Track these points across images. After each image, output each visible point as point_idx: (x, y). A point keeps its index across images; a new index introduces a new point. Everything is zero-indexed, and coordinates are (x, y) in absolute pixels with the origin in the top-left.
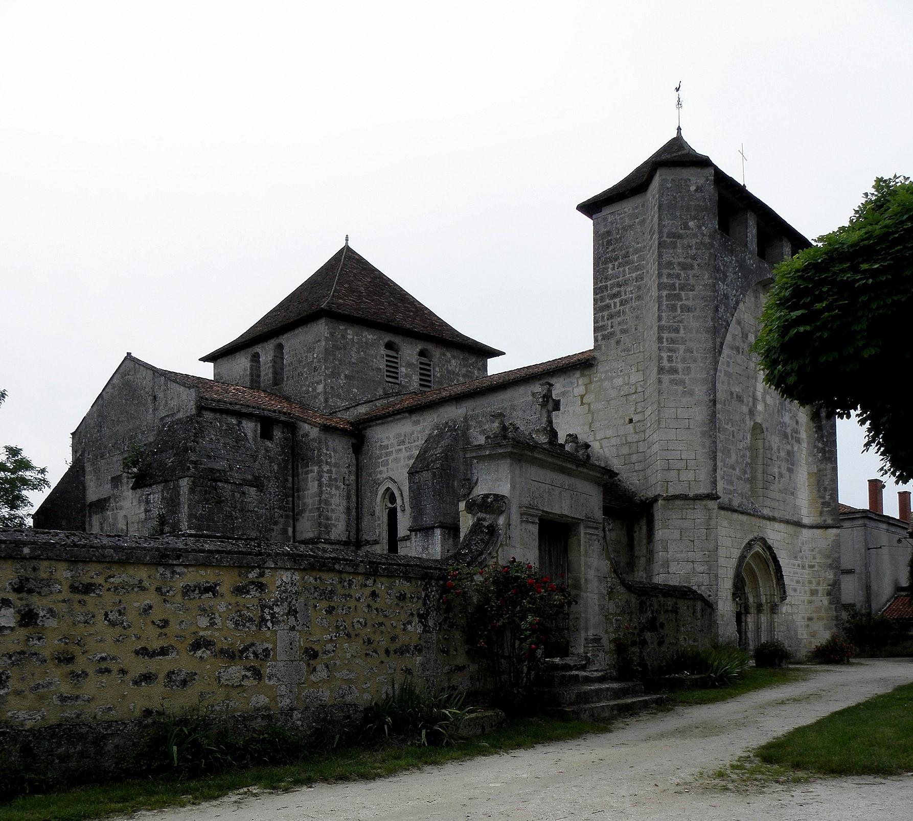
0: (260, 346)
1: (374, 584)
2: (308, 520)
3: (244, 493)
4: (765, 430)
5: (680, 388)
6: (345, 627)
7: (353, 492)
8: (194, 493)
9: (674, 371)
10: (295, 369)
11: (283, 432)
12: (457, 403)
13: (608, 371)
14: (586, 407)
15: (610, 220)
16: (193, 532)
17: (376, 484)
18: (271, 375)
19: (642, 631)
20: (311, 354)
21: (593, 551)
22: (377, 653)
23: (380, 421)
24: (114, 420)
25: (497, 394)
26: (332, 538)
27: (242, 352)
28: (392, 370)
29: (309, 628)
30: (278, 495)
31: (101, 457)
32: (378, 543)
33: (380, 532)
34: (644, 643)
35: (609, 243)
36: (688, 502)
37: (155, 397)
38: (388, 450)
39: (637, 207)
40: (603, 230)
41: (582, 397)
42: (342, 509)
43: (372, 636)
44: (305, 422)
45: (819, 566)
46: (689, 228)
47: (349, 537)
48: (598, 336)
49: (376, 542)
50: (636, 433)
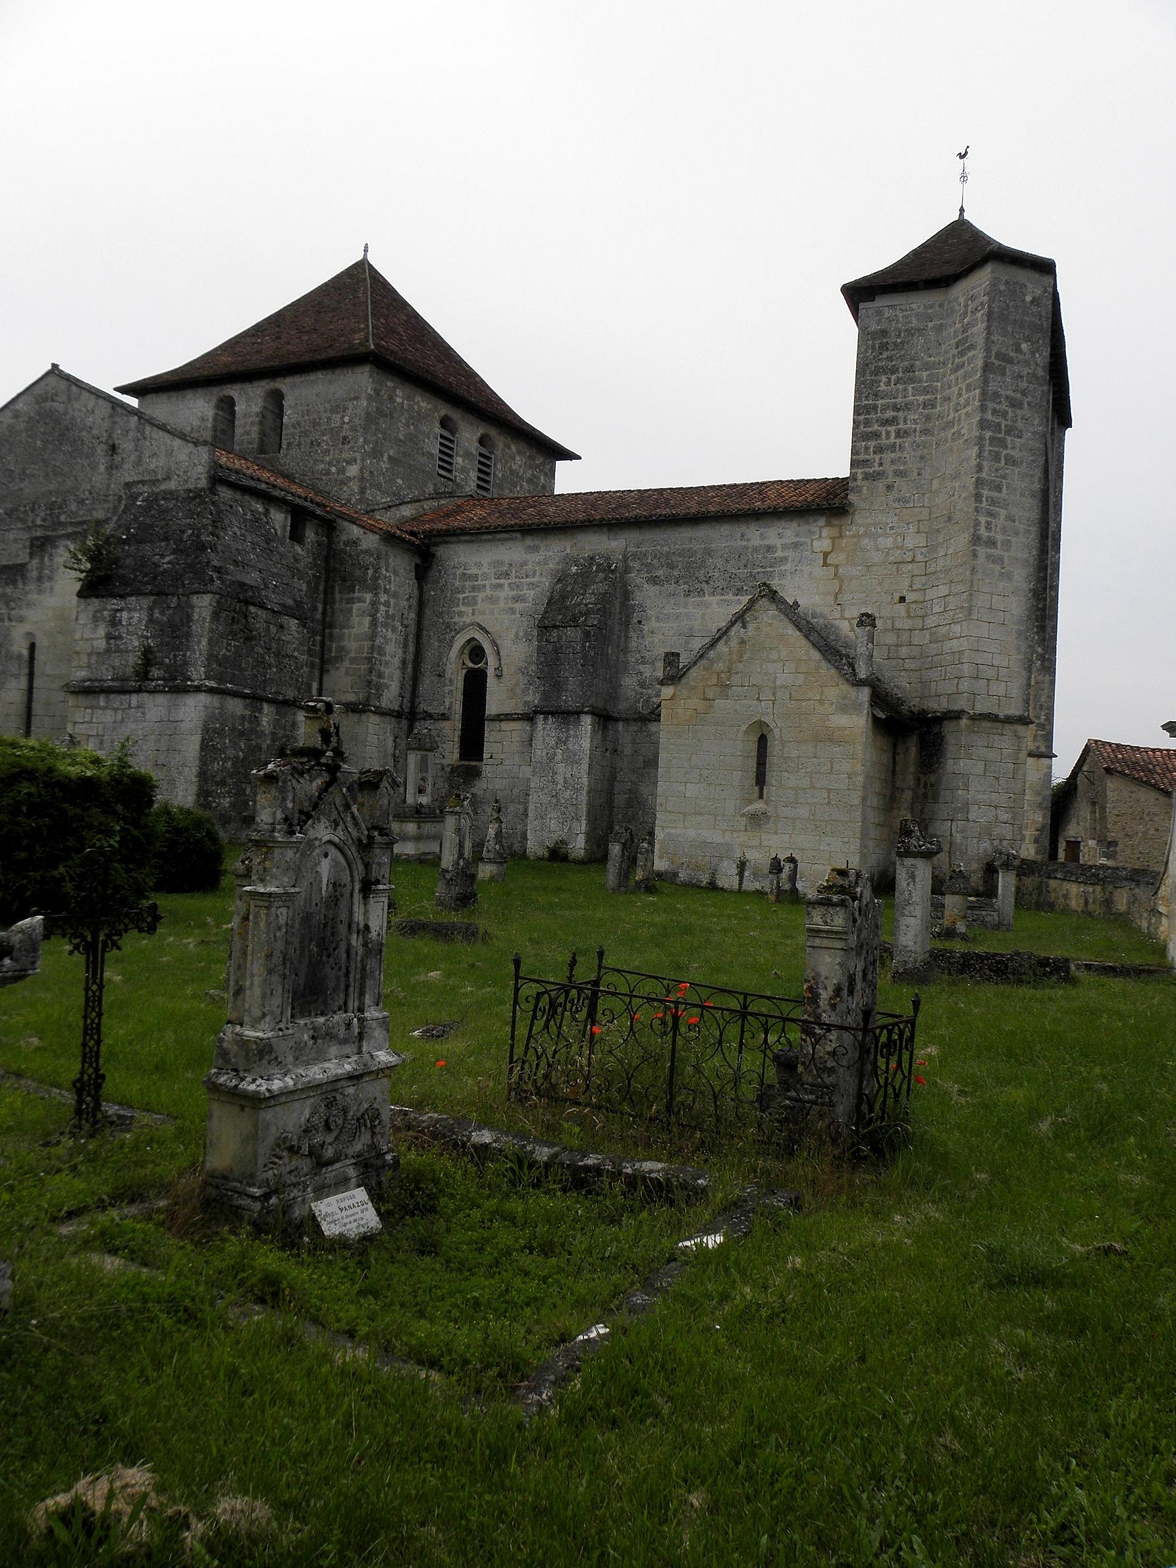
0: (237, 387)
2: (347, 674)
3: (282, 627)
7: (411, 638)
8: (218, 620)
9: (992, 543)
10: (305, 433)
11: (317, 534)
12: (609, 530)
13: (869, 525)
15: (886, 315)
16: (213, 684)
18: (255, 436)
25: (681, 529)
27: (200, 391)
32: (448, 719)
35: (884, 347)
36: (995, 724)
37: (113, 448)
39: (931, 307)
41: (826, 555)
42: (396, 661)
44: (354, 523)
47: (401, 706)
49: (444, 717)
50: (909, 617)
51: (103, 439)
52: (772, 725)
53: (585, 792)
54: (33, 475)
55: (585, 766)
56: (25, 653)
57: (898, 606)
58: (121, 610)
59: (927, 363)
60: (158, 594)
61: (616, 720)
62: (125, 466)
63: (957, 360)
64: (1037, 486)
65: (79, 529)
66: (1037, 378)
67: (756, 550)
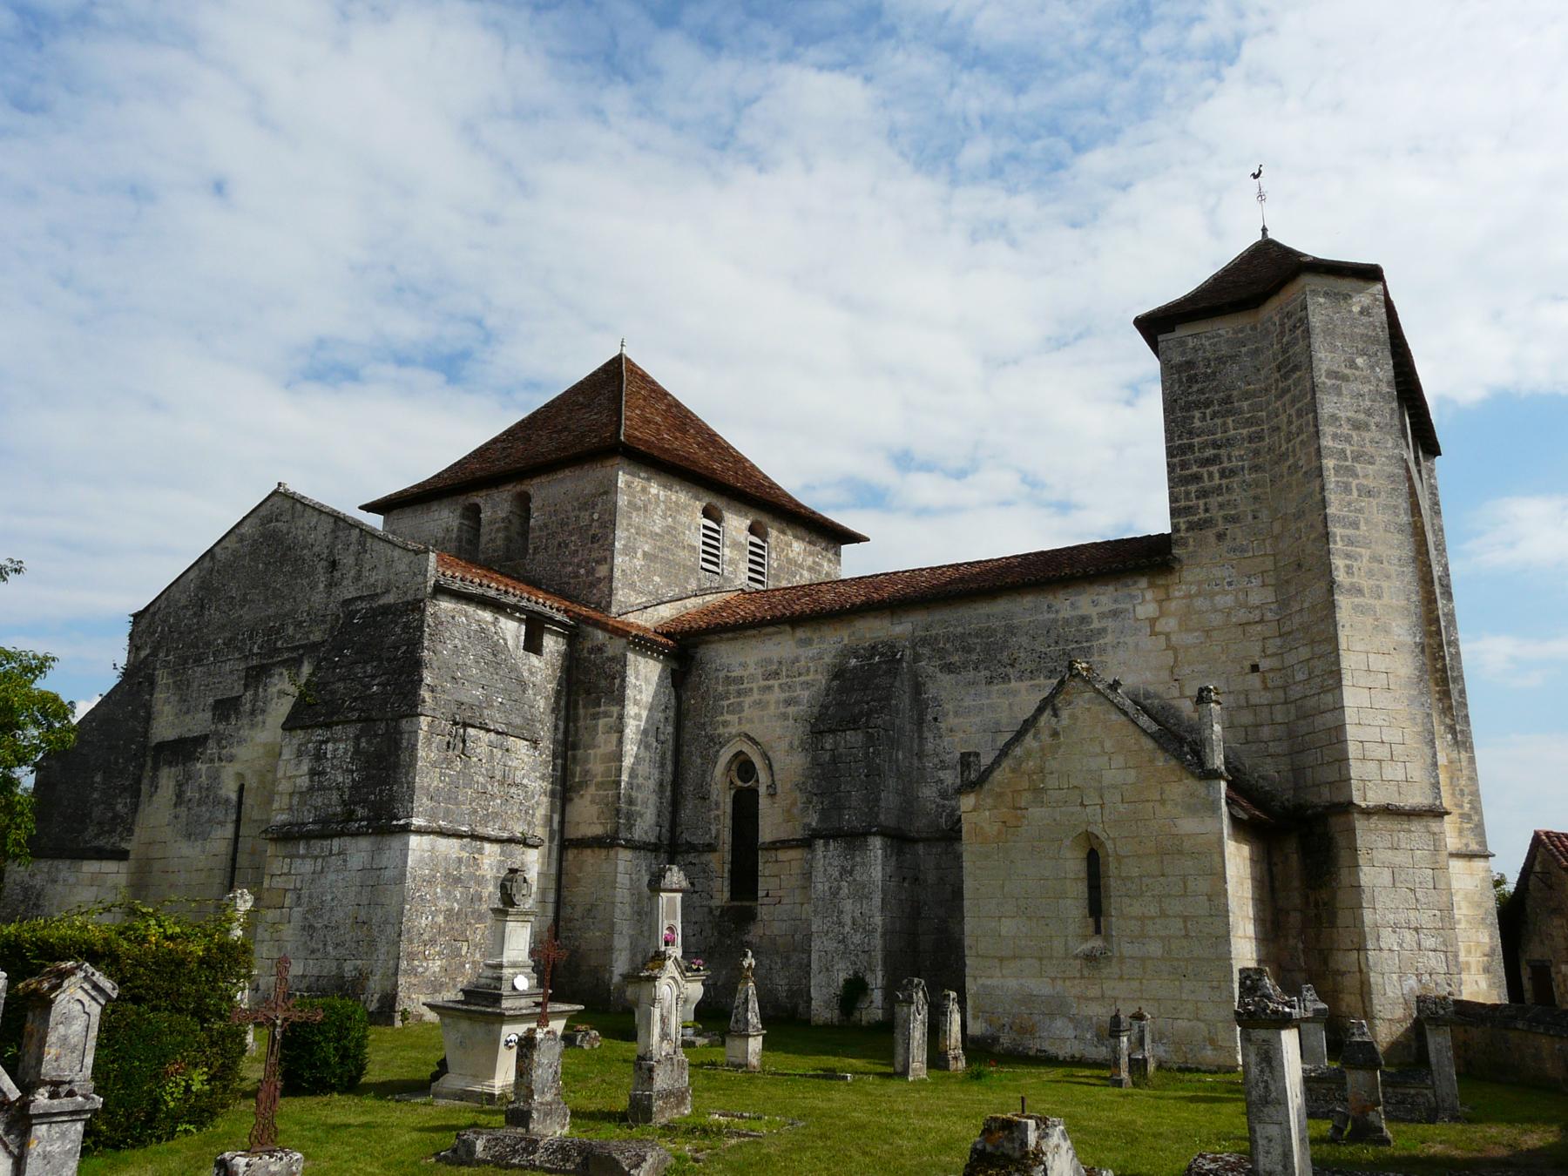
0: (483, 493)
2: (592, 802)
5: (1370, 621)
7: (669, 755)
9: (1359, 591)
10: (553, 535)
12: (893, 613)
15: (1191, 345)
23: (730, 635)
24: (234, 598)
26: (636, 837)
27: (445, 502)
31: (195, 661)
32: (715, 850)
33: (718, 830)
35: (1193, 379)
37: (333, 565)
39: (1241, 331)
45: (1467, 921)
46: (1357, 368)
47: (659, 838)
49: (710, 848)
50: (1266, 688)
51: (324, 556)
52: (1103, 836)
53: (878, 935)
54: (252, 601)
55: (877, 899)
56: (234, 796)
57: (1250, 677)
58: (326, 742)
59: (1247, 392)
60: (366, 720)
61: (915, 841)
62: (345, 583)
63: (1281, 385)
64: (1404, 519)
65: (295, 655)
66: (1383, 396)
67: (1067, 622)
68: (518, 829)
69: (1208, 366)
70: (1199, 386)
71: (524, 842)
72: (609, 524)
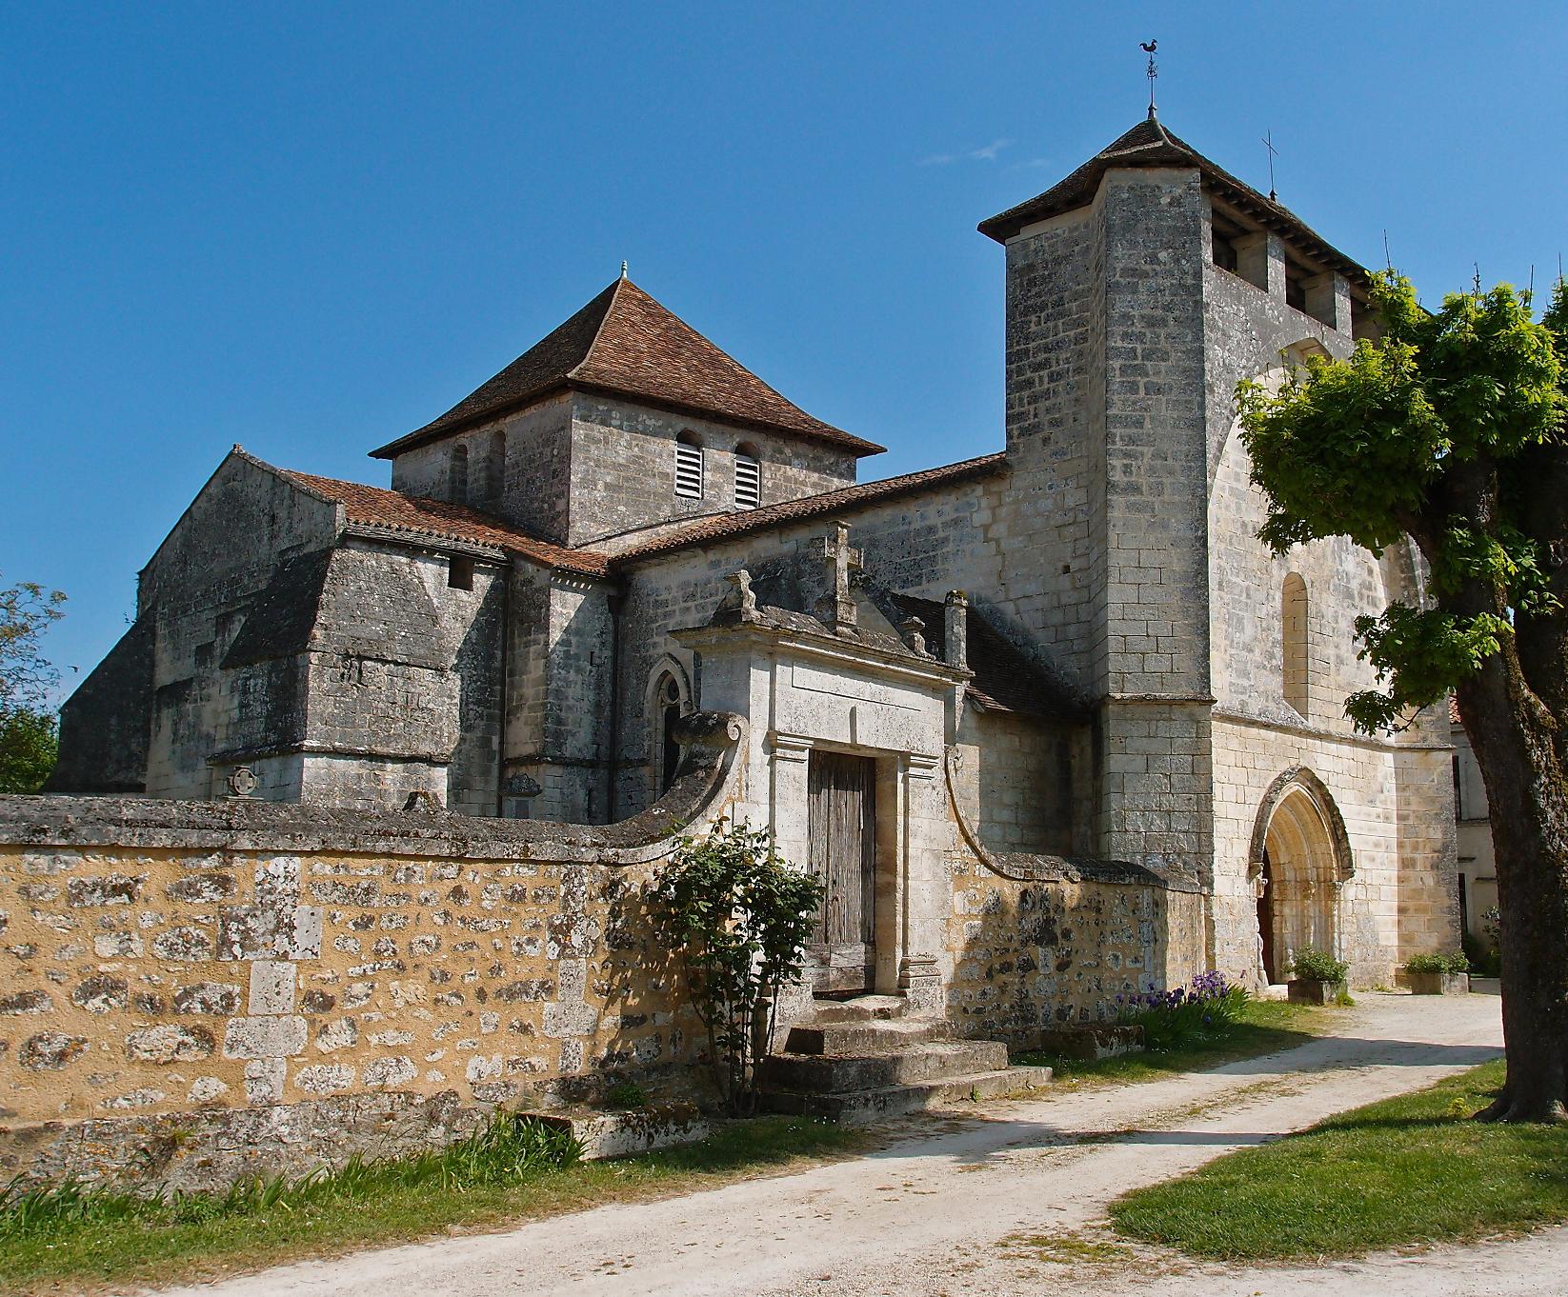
0: (467, 435)
1: (458, 874)
2: (526, 724)
4: (1308, 585)
6: (394, 952)
7: (607, 677)
9: (1136, 489)
14: (993, 544)
15: (1032, 247)
17: (647, 665)
19: (1024, 943)
20: (549, 450)
21: (922, 806)
22: (459, 997)
28: (747, 471)
29: (316, 954)
30: (475, 682)
32: (647, 765)
33: (650, 745)
34: (1028, 966)
35: (1032, 282)
36: (1160, 709)
37: (273, 518)
38: (667, 609)
40: (1021, 263)
42: (586, 705)
43: (450, 967)
47: (597, 754)
48: (1012, 429)
49: (643, 762)
50: (1075, 588)
58: (249, 679)
67: (918, 533)
68: (425, 748)
69: (1046, 268)
70: (1037, 289)
71: (430, 761)
72: (566, 460)
